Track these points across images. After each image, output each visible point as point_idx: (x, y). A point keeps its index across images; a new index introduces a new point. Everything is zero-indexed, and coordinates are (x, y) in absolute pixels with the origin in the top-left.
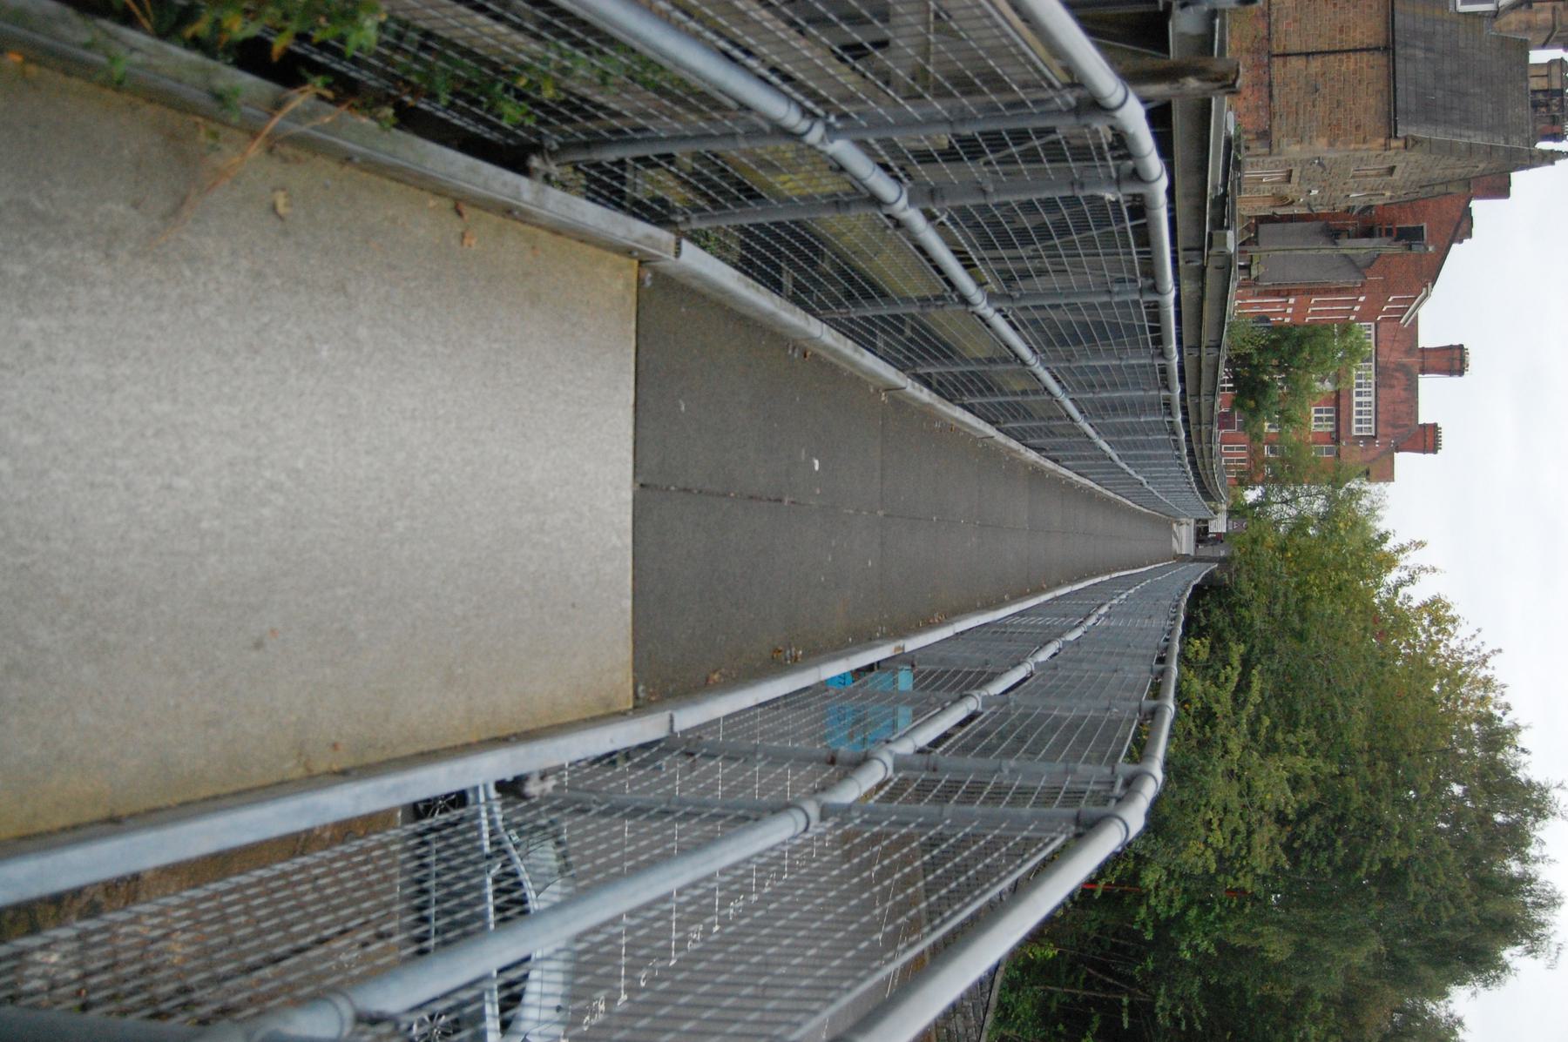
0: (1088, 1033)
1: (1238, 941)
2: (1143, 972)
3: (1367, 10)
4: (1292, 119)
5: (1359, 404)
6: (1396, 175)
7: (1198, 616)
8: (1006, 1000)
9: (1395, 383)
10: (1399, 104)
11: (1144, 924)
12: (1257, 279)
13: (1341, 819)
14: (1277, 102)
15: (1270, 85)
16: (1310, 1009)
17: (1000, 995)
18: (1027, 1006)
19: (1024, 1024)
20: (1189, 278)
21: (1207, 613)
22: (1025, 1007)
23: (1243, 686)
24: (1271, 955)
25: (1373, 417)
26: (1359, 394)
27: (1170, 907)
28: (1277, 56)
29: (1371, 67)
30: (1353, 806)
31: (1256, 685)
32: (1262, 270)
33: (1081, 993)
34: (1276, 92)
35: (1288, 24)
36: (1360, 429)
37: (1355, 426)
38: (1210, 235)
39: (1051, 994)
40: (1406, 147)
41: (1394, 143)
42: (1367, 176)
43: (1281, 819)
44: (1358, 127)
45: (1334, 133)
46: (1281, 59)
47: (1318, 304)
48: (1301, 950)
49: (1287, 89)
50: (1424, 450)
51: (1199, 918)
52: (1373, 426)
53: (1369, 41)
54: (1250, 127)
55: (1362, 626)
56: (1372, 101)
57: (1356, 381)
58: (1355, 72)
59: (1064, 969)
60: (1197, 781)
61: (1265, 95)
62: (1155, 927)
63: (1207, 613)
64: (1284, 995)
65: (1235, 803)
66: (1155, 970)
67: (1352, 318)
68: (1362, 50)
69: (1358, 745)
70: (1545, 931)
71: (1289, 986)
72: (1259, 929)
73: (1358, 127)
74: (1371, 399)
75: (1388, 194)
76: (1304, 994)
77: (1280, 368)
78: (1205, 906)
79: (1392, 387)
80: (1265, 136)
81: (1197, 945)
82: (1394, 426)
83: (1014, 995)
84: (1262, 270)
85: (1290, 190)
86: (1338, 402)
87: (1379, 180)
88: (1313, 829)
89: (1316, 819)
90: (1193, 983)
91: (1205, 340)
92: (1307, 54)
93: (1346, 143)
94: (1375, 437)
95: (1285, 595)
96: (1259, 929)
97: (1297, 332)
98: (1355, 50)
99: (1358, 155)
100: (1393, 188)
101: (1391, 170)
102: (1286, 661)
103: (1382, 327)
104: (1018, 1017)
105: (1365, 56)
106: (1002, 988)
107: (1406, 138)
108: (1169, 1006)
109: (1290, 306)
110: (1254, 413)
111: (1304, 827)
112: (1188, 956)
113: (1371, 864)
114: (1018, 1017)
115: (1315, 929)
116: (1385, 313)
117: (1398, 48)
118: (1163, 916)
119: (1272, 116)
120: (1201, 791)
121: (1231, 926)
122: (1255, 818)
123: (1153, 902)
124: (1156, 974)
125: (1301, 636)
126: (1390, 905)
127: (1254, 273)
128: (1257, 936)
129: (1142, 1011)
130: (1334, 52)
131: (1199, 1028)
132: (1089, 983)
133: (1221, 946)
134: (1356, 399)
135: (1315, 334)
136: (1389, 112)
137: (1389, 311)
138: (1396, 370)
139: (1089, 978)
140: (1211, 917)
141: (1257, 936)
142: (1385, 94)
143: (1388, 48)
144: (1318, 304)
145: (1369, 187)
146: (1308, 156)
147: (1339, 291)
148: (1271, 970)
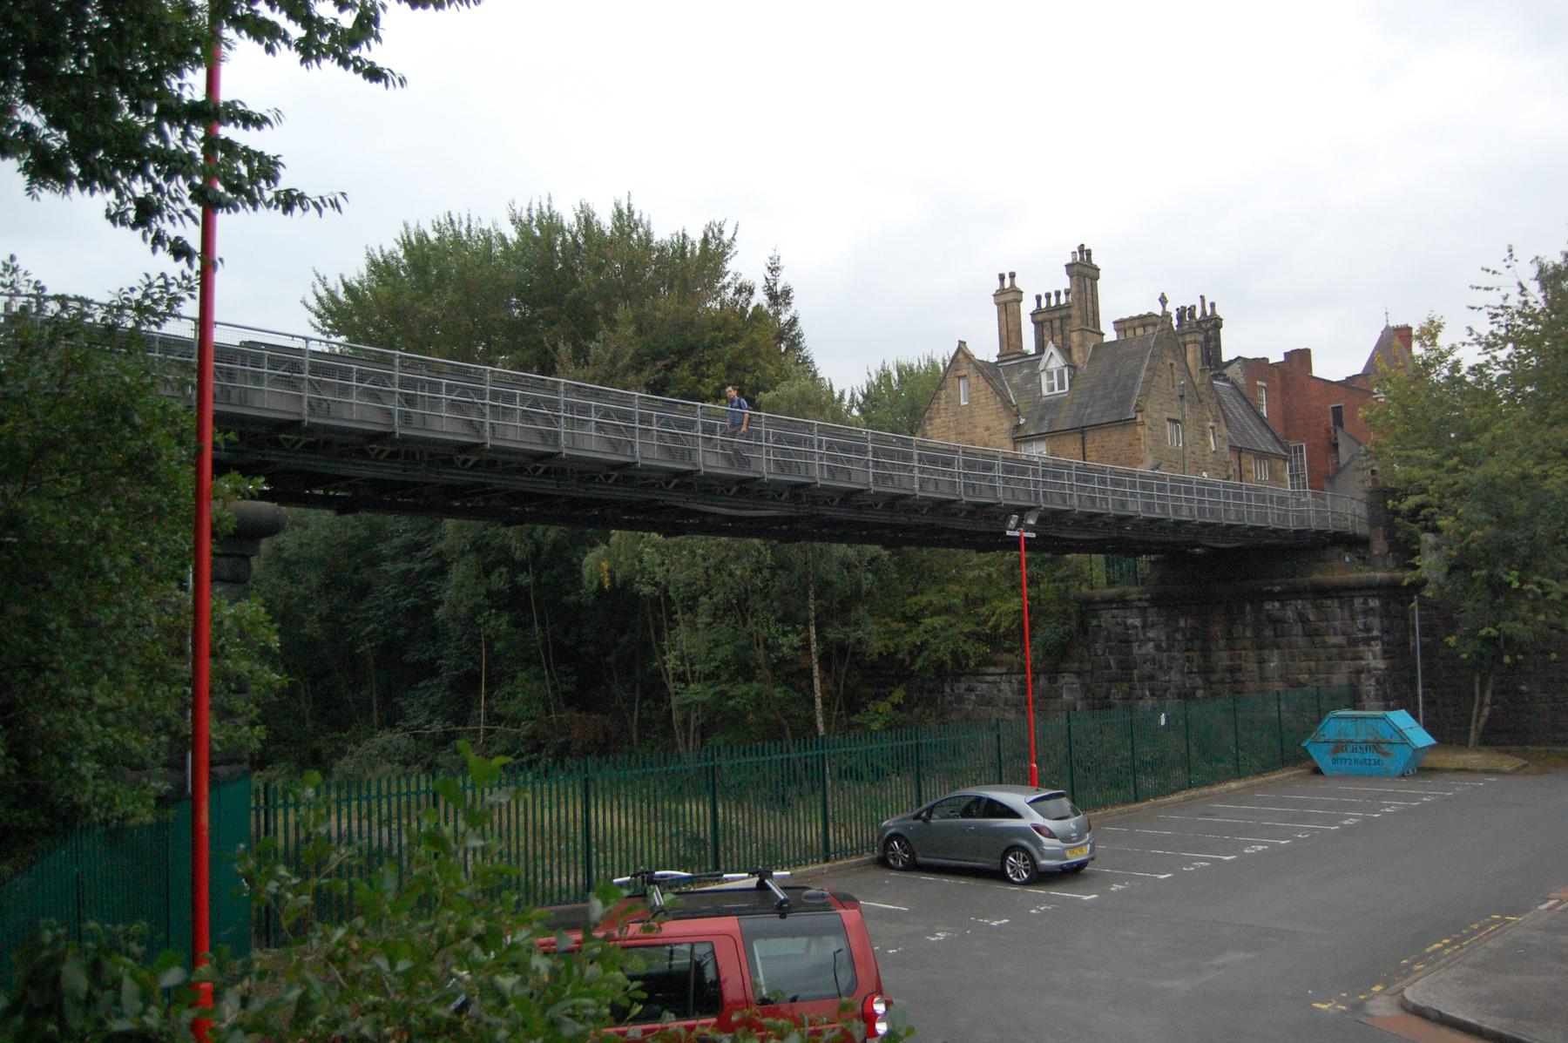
41: (1139, 419)
50: (1122, 321)
53: (1079, 445)
56: (1115, 438)
57: (1056, 391)
70: (241, 127)
93: (1141, 451)
105: (1087, 446)
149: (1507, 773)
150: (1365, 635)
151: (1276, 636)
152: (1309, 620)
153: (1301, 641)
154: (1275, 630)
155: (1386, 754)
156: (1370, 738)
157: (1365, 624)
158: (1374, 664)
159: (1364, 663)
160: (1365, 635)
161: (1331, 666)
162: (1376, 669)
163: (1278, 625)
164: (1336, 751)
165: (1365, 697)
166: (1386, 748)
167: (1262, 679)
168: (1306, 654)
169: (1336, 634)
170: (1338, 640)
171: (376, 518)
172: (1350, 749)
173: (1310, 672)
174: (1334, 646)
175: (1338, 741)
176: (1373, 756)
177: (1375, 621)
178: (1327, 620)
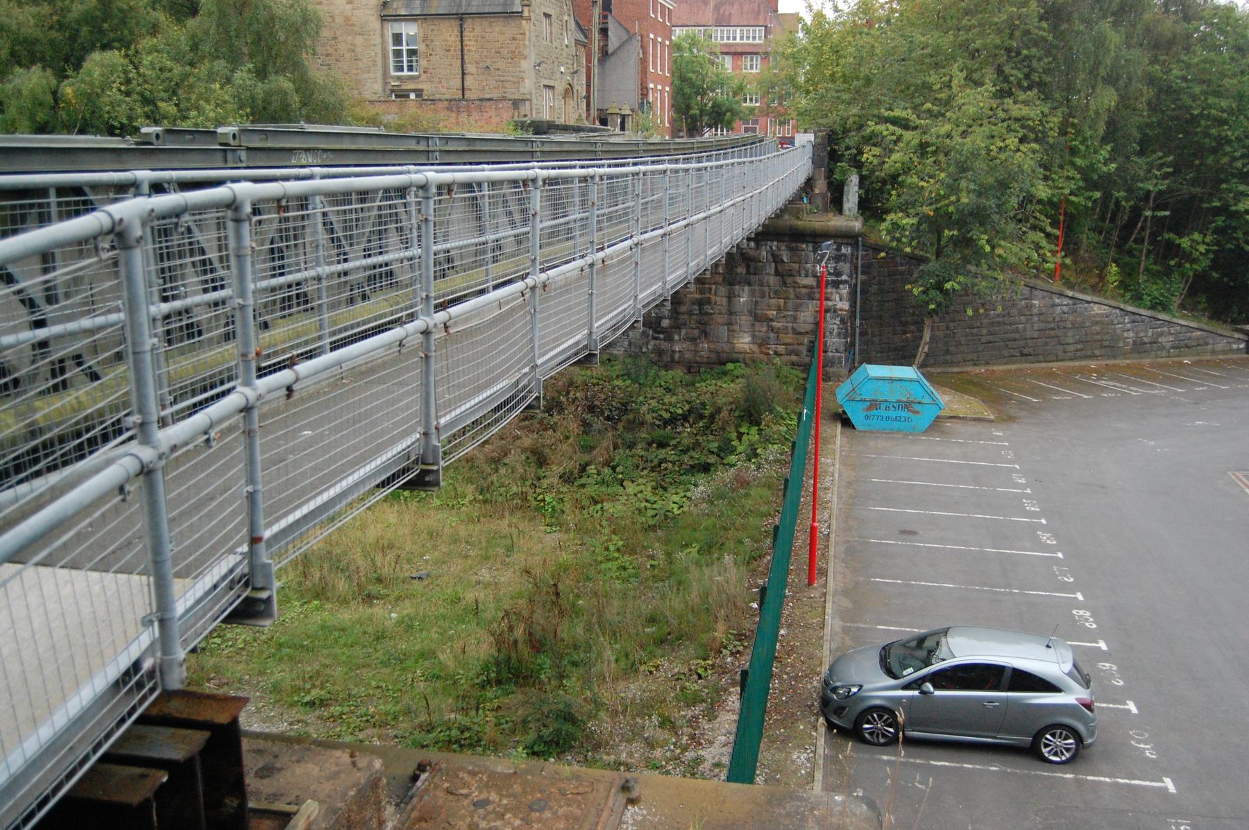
0: (1177, 242)
1: (1102, 129)
2: (1127, 200)
3: (435, 32)
4: (507, 85)
5: (742, 38)
6: (549, 11)
7: (850, 155)
8: (1148, 303)
9: (727, 12)
10: (498, 10)
11: (1089, 198)
12: (632, 110)
13: (1009, 50)
14: (495, 96)
15: (481, 100)
16: (1160, 74)
17: (1144, 308)
18: (1154, 287)
19: (1168, 290)
20: (291, 159)
21: (848, 148)
22: (1155, 289)
23: (905, 124)
24: (1113, 103)
25: (751, 29)
26: (735, 38)
27: (1073, 178)
28: (463, 95)
29: (474, 29)
30: (998, 41)
31: (898, 113)
32: (626, 106)
33: (1146, 245)
34: (488, 96)
35: (443, 87)
36: (760, 37)
37: (757, 41)
38: (221, 144)
39: (1147, 269)
40: (528, 6)
41: (526, 14)
42: (551, 33)
43: (1002, 94)
44: (514, 39)
45: (516, 56)
46: (466, 92)
47: (655, 67)
48: (1111, 80)
49: (487, 88)
51: (1084, 157)
52: (757, 29)
54: (510, 114)
55: (858, 36)
56: (497, 29)
58: (477, 41)
59: (1127, 259)
60: (967, 157)
61: (489, 103)
62: (1090, 190)
63: (848, 148)
64: (1148, 93)
65: (986, 129)
66: (1127, 191)
67: (667, 43)
68: (462, 37)
69: (952, 38)
71: (1140, 90)
72: (1092, 113)
73: (514, 39)
74: (738, 29)
75: (566, 18)
76: (1151, 80)
77: (704, 94)
78: (1073, 151)
79: (730, 15)
80: (516, 104)
81: (1104, 158)
82: (759, 13)
83: (1145, 297)
84: (626, 106)
85: (560, 87)
86: (737, 54)
87: (554, 24)
88: (1014, 72)
89: (1007, 69)
90: (1136, 163)
91: (422, 147)
92: (463, 74)
94: (766, 27)
95: (838, 91)
96: (1092, 113)
97: (677, 82)
98: (462, 41)
99: (533, 39)
100: (562, 14)
101: (547, 16)
102: (885, 91)
103: (674, 21)
104: (1162, 295)
106: (1139, 307)
107: (523, 6)
108: (1154, 181)
109: (656, 86)
110: (734, 113)
111: (1012, 79)
112: (1113, 166)
113: (1044, 30)
114: (1162, 295)
115: (1093, 72)
116: (664, 21)
117: (461, 11)
118: (1081, 184)
119: (504, 99)
120: (975, 155)
121: (1089, 133)
122: (1001, 115)
123: (1067, 191)
124: (1130, 190)
125: (868, 81)
126: (1075, 15)
127: (628, 112)
128: (1097, 113)
129: (1161, 201)
130: (462, 55)
131: (1171, 158)
132: (1139, 241)
133: (1105, 140)
134: (738, 40)
135: (679, 69)
136: (505, 17)
137: (663, 16)
138: (719, 12)
139: (1136, 241)
140: (1083, 148)
141: (1097, 113)
142: (492, 20)
143: (461, 17)
144: (655, 67)
145: (560, 31)
146: (533, 74)
147: (645, 53)
148: (1125, 102)
149: (991, 421)
150: (834, 278)
151: (748, 272)
152: (782, 261)
153: (772, 280)
154: (748, 267)
155: (917, 412)
156: (904, 399)
157: (835, 268)
158: (839, 305)
159: (830, 303)
160: (834, 278)
161: (801, 305)
162: (841, 310)
163: (752, 264)
164: (869, 409)
165: (828, 334)
166: (916, 407)
167: (731, 313)
168: (776, 292)
169: (807, 276)
170: (810, 281)
171: (133, 380)
172: (883, 407)
173: (779, 309)
174: (805, 287)
175: (873, 400)
176: (904, 413)
177: (845, 267)
178: (800, 263)
